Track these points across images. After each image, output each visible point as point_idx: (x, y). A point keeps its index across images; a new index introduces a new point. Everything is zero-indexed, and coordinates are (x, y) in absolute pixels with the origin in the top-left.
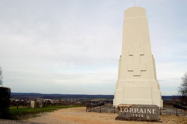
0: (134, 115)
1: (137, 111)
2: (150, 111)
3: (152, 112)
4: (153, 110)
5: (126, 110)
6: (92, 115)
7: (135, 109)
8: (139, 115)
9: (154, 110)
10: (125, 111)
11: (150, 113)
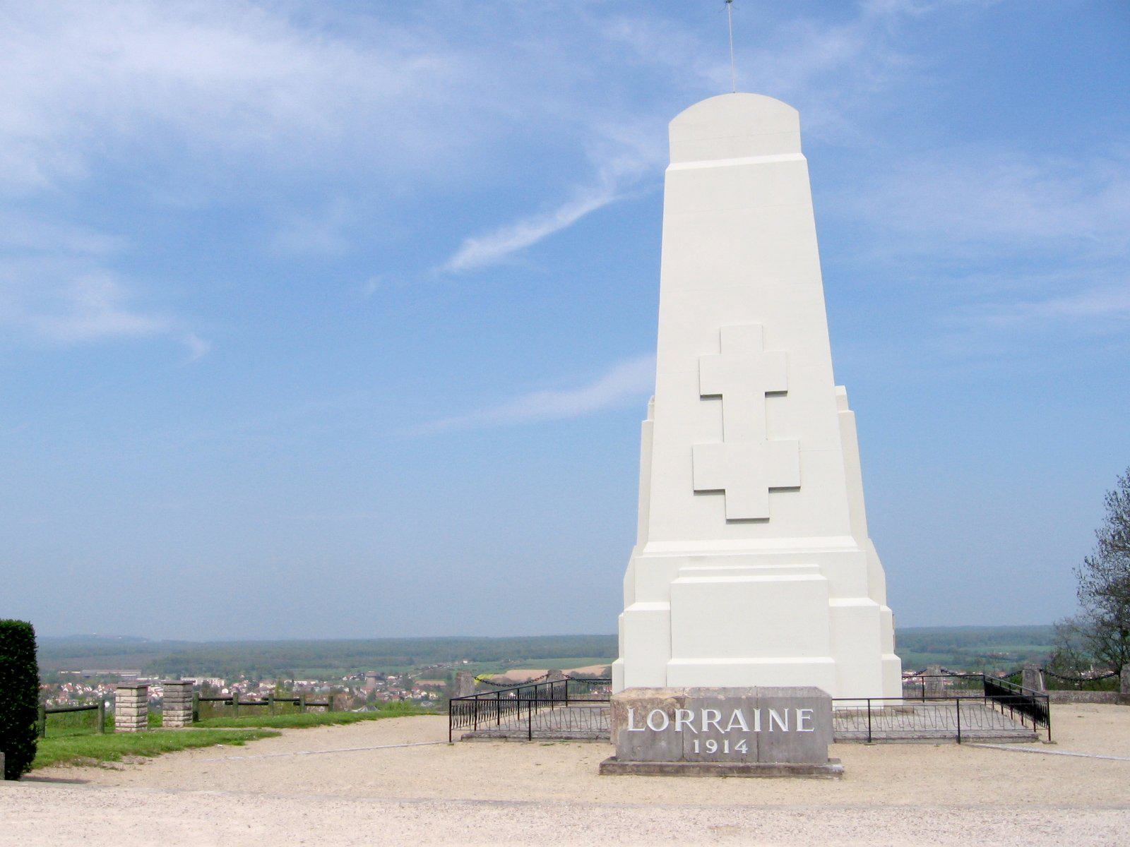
3: (796, 725)
7: (705, 713)
10: (650, 724)
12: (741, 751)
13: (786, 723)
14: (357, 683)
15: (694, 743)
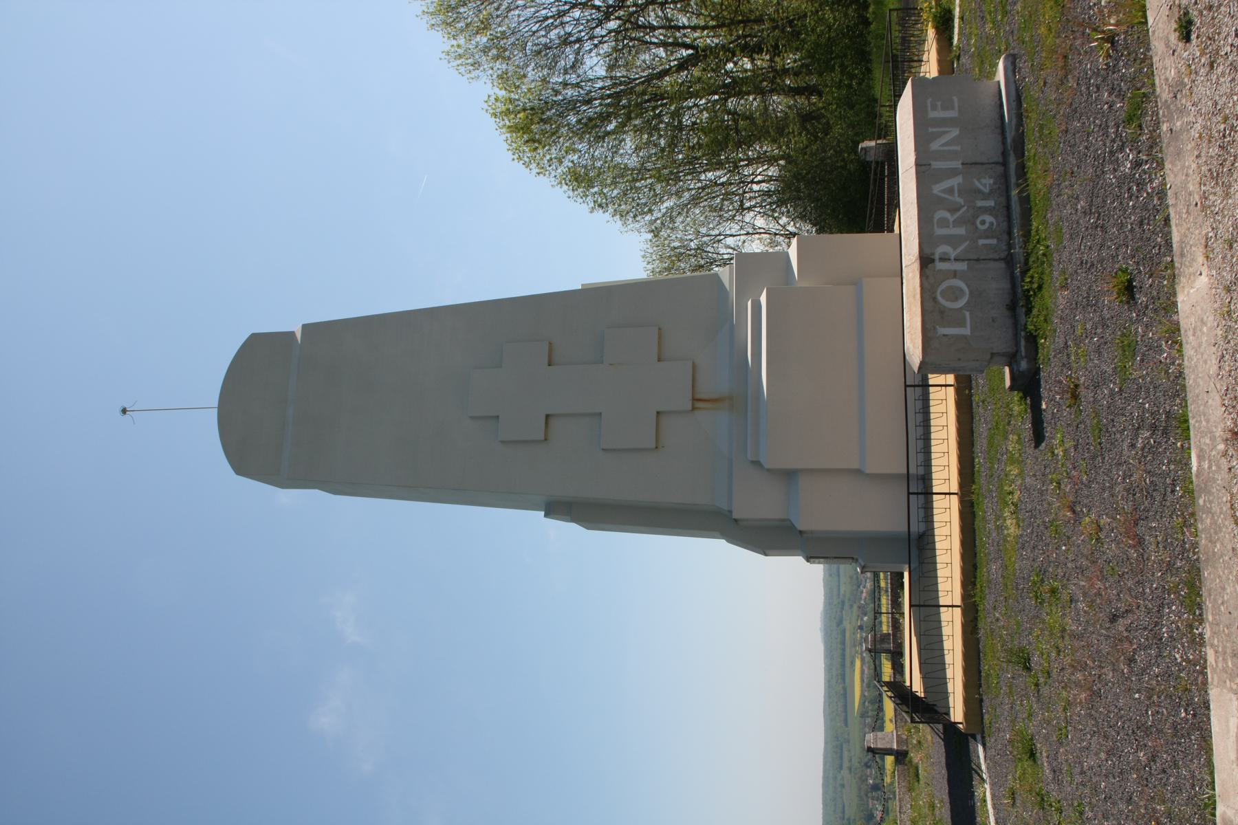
0: (981, 242)
1: (951, 218)
2: (940, 135)
3: (951, 119)
4: (933, 114)
5: (954, 294)
6: (981, 410)
7: (940, 232)
8: (980, 203)
9: (934, 108)
10: (960, 304)
11: (955, 132)
12: (990, 184)
13: (942, 148)
14: (1155, 169)
15: (983, 245)
